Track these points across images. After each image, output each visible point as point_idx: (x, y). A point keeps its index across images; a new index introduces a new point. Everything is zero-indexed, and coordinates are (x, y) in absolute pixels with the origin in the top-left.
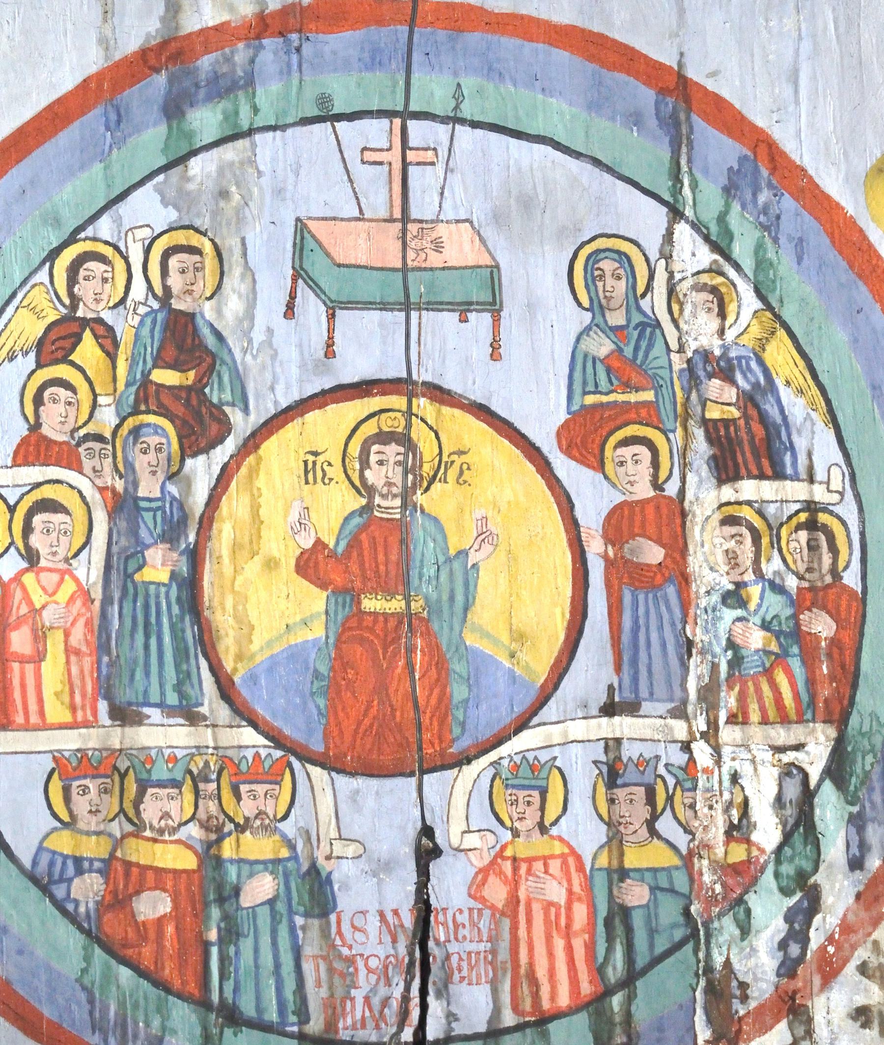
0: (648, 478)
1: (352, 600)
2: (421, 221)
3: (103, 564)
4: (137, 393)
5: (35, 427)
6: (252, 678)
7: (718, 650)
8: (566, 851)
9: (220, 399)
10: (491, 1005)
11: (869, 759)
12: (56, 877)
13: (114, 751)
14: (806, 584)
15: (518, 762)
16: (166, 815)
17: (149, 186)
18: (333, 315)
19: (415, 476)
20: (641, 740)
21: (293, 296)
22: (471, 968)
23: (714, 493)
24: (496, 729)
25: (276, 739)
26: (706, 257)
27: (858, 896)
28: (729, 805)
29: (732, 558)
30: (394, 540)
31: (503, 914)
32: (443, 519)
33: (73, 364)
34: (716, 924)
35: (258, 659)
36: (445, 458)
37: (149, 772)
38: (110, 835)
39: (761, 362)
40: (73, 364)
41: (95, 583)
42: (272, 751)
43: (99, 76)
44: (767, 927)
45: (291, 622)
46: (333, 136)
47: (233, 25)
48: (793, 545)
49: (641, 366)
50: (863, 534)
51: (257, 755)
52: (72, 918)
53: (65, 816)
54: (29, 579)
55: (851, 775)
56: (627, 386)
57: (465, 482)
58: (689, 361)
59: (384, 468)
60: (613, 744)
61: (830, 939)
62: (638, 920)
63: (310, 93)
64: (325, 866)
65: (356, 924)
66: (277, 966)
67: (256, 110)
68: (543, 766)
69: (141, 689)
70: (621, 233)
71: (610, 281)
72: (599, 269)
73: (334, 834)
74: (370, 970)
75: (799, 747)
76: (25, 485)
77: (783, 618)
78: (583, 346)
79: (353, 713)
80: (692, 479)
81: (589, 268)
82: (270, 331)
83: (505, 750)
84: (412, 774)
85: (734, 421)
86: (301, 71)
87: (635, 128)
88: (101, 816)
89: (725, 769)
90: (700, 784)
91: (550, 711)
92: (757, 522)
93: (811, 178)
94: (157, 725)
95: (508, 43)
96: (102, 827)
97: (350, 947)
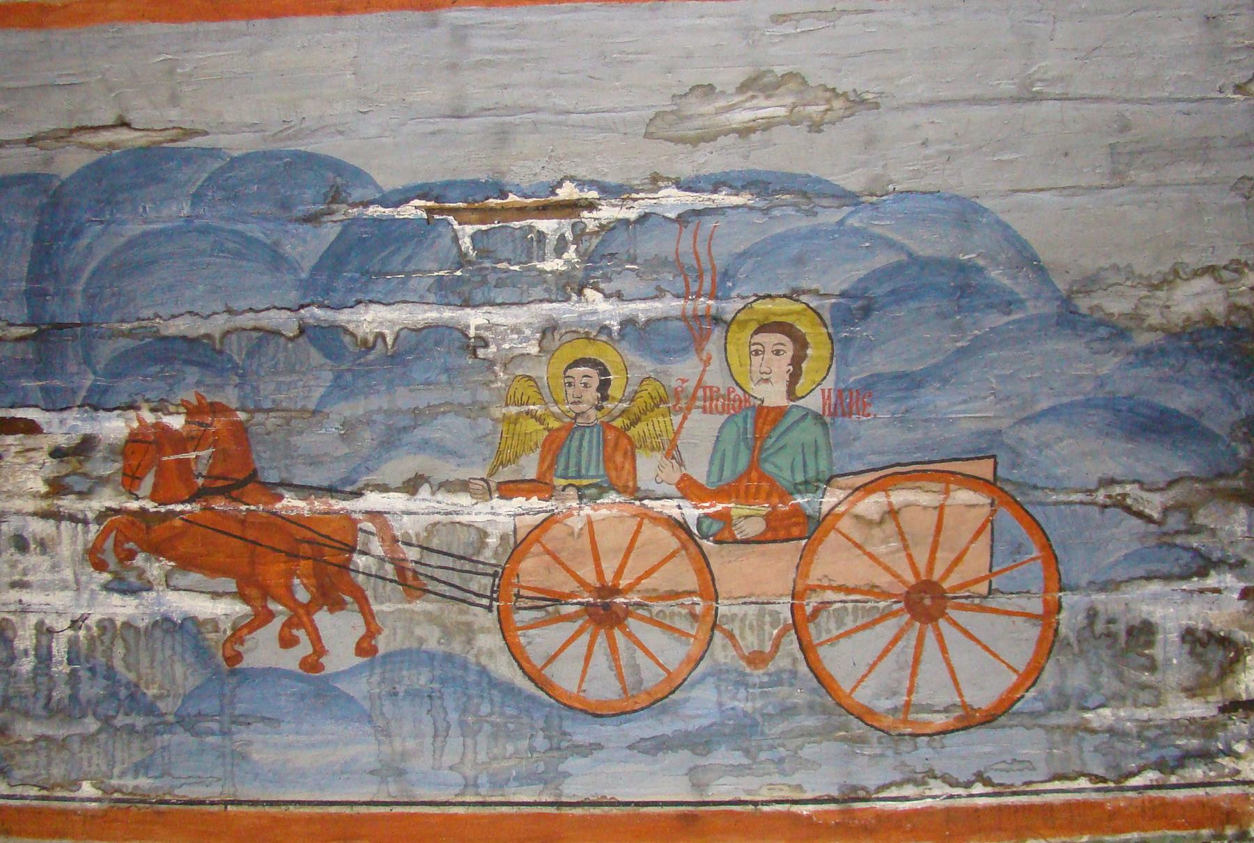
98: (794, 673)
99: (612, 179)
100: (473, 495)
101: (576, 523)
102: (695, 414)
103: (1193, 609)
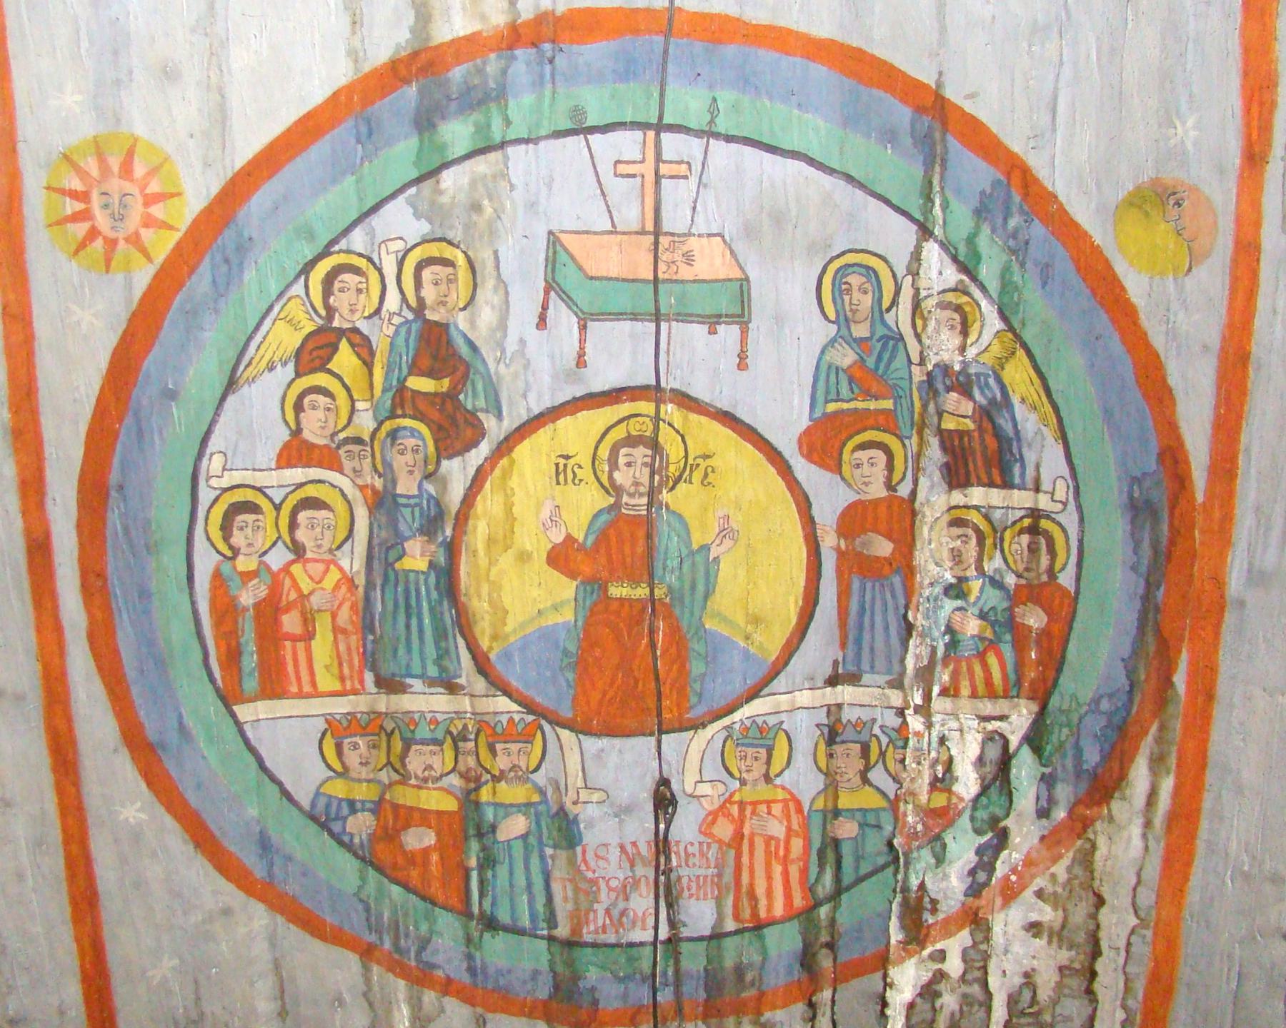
0: (882, 480)
1: (600, 587)
2: (672, 234)
3: (365, 554)
4: (393, 399)
5: (297, 432)
6: (507, 655)
7: (936, 634)
8: (789, 797)
9: (474, 405)
10: (715, 916)
11: (1065, 731)
12: (333, 816)
13: (380, 714)
14: (1023, 582)
15: (749, 725)
16: (429, 767)
17: (401, 199)
18: (585, 327)
19: (661, 477)
20: (861, 706)
21: (545, 307)
22: (699, 887)
23: (944, 497)
24: (729, 700)
25: (529, 706)
26: (952, 276)
27: (1043, 838)
28: (936, 761)
29: (957, 557)
30: (641, 534)
31: (729, 846)
32: (687, 515)
33: (330, 372)
34: (915, 855)
35: (512, 639)
36: (690, 461)
37: (413, 732)
38: (379, 782)
40: (330, 372)
41: (358, 572)
42: (524, 716)
43: (349, 90)
44: (959, 859)
45: (542, 607)
46: (586, 149)
47: (485, 34)
48: (1015, 547)
49: (881, 377)
50: (1081, 542)
51: (511, 720)
52: (349, 847)
53: (338, 767)
54: (296, 569)
55: (1047, 743)
56: (868, 394)
57: (709, 483)
58: (929, 374)
59: (631, 470)
60: (835, 709)
61: (1014, 871)
62: (846, 849)
63: (564, 105)
64: (572, 810)
65: (599, 853)
66: (529, 886)
67: (508, 122)
68: (770, 729)
69: (404, 662)
70: (870, 249)
71: (856, 295)
72: (846, 283)
73: (580, 783)
74: (610, 889)
75: (1002, 718)
76: (289, 485)
77: (999, 609)
78: (827, 357)
79: (600, 684)
80: (924, 482)
81: (837, 282)
82: (522, 342)
83: (737, 716)
84: (652, 734)
85: (968, 432)
86: (553, 83)
87: (889, 145)
88: (371, 767)
89: (935, 734)
90: (911, 743)
91: (780, 683)
92: (983, 525)
93: (1061, 206)
94: (420, 693)
95: (765, 57)
96: (372, 776)
97: (594, 872)
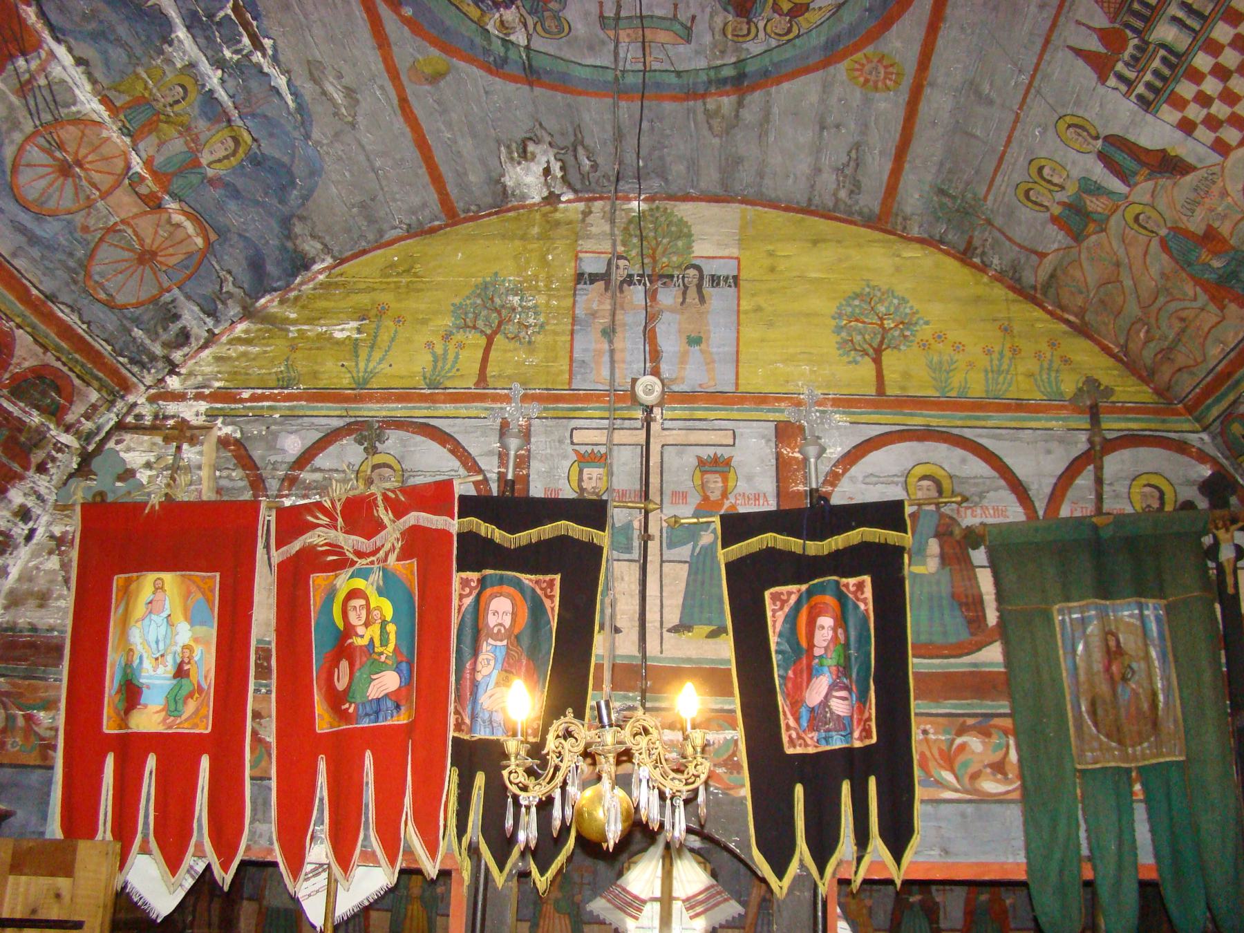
26: (513, 38)
39: (482, 10)
98: (88, 244)
99: (281, 58)
100: (94, 89)
101: (105, 134)
102: (182, 141)
103: (194, 322)
